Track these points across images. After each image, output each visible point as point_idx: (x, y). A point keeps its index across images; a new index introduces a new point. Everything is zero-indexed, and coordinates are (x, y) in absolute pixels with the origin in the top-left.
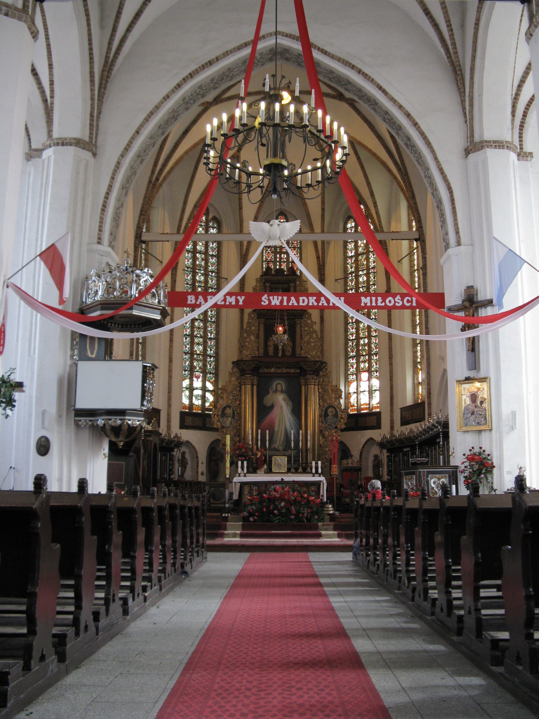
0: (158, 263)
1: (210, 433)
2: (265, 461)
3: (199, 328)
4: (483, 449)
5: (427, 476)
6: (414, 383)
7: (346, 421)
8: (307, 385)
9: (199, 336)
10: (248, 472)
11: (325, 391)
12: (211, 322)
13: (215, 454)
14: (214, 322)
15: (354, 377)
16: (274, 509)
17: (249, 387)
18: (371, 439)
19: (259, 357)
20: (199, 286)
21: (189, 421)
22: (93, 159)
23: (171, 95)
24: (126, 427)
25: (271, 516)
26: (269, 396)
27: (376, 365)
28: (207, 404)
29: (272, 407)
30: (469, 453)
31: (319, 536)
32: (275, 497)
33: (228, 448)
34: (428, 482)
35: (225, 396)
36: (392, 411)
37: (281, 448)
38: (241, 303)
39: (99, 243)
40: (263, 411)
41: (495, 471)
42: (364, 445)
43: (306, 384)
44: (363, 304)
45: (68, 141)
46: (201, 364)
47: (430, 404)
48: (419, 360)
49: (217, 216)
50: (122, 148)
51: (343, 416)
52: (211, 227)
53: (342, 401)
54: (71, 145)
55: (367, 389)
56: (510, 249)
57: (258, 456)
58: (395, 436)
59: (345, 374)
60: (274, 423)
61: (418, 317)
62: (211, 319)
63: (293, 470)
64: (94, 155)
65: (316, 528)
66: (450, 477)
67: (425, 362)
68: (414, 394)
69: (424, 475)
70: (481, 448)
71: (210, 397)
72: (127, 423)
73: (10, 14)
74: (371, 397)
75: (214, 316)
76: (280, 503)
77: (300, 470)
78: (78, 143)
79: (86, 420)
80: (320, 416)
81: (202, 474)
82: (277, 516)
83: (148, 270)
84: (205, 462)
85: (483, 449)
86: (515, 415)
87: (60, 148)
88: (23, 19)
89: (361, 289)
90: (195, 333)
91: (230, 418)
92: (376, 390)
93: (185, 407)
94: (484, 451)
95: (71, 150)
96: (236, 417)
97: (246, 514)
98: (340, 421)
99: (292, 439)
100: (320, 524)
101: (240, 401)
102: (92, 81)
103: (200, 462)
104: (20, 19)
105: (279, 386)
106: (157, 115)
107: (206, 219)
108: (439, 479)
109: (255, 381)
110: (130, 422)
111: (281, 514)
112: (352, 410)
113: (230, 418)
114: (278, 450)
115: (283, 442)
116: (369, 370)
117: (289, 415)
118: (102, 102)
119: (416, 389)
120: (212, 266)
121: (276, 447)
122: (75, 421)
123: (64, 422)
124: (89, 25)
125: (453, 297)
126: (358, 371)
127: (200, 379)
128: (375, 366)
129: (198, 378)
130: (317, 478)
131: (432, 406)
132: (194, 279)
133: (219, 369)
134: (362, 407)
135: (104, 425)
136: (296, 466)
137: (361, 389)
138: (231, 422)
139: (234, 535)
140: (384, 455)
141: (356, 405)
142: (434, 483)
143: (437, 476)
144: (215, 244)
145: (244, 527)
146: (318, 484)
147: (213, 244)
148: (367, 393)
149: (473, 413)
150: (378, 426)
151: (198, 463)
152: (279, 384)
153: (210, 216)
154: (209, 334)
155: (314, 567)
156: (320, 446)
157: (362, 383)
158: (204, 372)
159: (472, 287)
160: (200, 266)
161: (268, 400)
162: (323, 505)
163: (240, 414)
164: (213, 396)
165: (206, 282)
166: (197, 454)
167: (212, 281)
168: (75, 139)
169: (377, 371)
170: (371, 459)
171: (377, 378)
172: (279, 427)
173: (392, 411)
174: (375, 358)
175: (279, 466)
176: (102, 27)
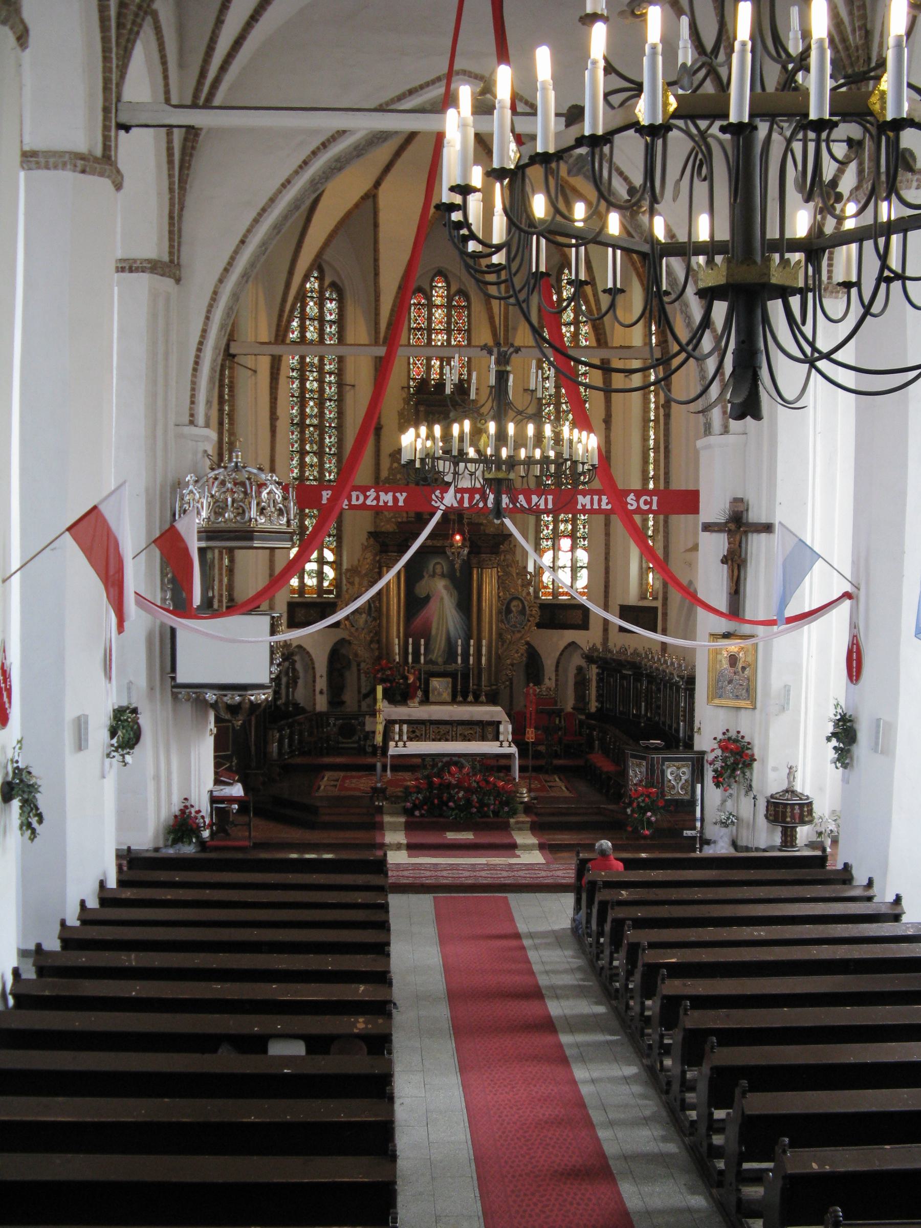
0: (250, 372)
3: (312, 466)
4: (742, 734)
5: (663, 764)
6: (641, 568)
7: (537, 620)
8: (482, 569)
9: (311, 478)
10: (410, 739)
11: (508, 574)
12: (330, 454)
14: (334, 454)
15: (550, 543)
16: (449, 800)
19: (408, 522)
20: (311, 399)
21: (300, 614)
22: (176, 287)
23: (294, 178)
24: (247, 706)
25: (445, 808)
26: (424, 582)
27: (584, 528)
28: (326, 584)
29: (428, 598)
30: (720, 737)
32: (450, 783)
34: (663, 772)
35: (357, 580)
37: (440, 660)
38: (401, 503)
39: (192, 423)
41: (755, 765)
42: (563, 651)
44: (579, 507)
45: (138, 264)
46: (308, 385)
47: (665, 615)
48: (650, 533)
49: (338, 281)
50: (220, 269)
51: (534, 612)
52: (328, 299)
54: (143, 272)
55: (569, 564)
56: (800, 540)
57: (410, 681)
58: (610, 651)
59: (536, 539)
60: (431, 623)
61: (651, 467)
62: (330, 449)
64: (178, 281)
66: (693, 765)
67: (660, 537)
68: (641, 584)
69: (658, 763)
70: (738, 732)
72: (249, 700)
73: (88, 169)
74: (574, 577)
75: (333, 446)
76: (458, 793)
77: (470, 698)
78: (153, 267)
79: (188, 693)
80: (499, 612)
81: (321, 692)
82: (453, 809)
83: (272, 477)
84: (325, 674)
85: (742, 734)
86: (789, 691)
87: (126, 275)
88: (107, 174)
89: (564, 406)
90: (307, 474)
91: (364, 616)
92: (582, 567)
94: (743, 737)
95: (145, 277)
98: (529, 621)
99: (459, 651)
100: (512, 821)
102: (170, 162)
104: (101, 175)
105: (438, 567)
106: (272, 212)
107: (321, 286)
108: (678, 768)
110: (252, 698)
111: (458, 807)
112: (544, 594)
113: (364, 616)
115: (444, 651)
116: (573, 536)
117: (454, 611)
118: (185, 190)
119: (645, 576)
120: (330, 364)
121: (434, 658)
122: (173, 693)
123: (158, 703)
124: (166, 78)
125: (713, 507)
126: (556, 536)
128: (582, 530)
130: (506, 750)
131: (668, 617)
132: (302, 387)
133: (343, 529)
134: (561, 590)
135: (216, 701)
137: (560, 563)
138: (366, 621)
141: (551, 587)
142: (671, 774)
143: (676, 764)
144: (334, 327)
146: (509, 756)
147: (331, 327)
148: (568, 570)
149: (730, 682)
151: (314, 677)
152: (438, 563)
153: (327, 283)
154: (327, 475)
155: (532, 955)
157: (561, 554)
159: (741, 500)
160: (312, 365)
161: (421, 589)
164: (334, 569)
165: (321, 390)
166: (313, 663)
167: (330, 388)
168: (149, 261)
169: (584, 539)
170: (572, 672)
171: (585, 549)
172: (438, 629)
174: (583, 517)
176: (182, 66)
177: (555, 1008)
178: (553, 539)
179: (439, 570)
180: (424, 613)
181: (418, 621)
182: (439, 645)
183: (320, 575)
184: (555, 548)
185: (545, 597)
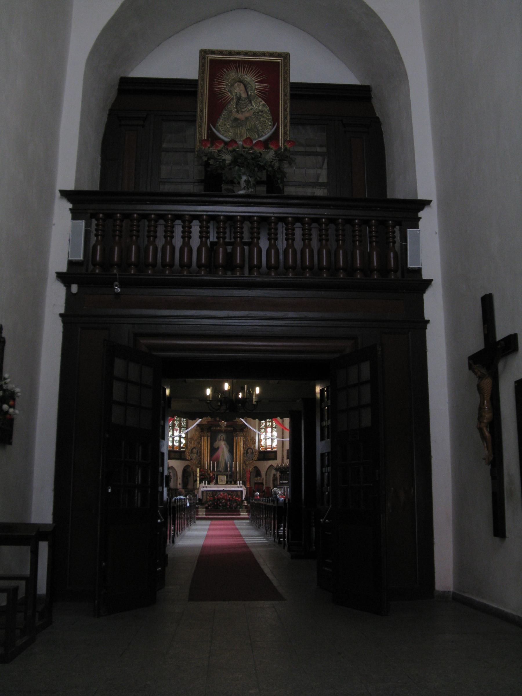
1: (184, 461)
2: (214, 478)
11: (246, 440)
13: (186, 472)
15: (264, 430)
17: (206, 438)
18: (272, 465)
21: (172, 455)
26: (217, 442)
28: (182, 445)
29: (218, 448)
31: (240, 515)
33: (198, 475)
35: (193, 442)
36: (283, 451)
37: (223, 471)
40: (213, 450)
43: (237, 437)
46: (178, 423)
53: (257, 445)
63: (229, 483)
65: (239, 511)
71: (183, 441)
77: (233, 482)
80: (244, 453)
81: (180, 484)
93: (170, 447)
96: (199, 454)
97: (207, 505)
101: (201, 445)
103: (178, 478)
105: (222, 437)
109: (209, 434)
111: (223, 506)
114: (221, 472)
116: (272, 427)
126: (266, 427)
127: (178, 431)
129: (177, 430)
136: (230, 480)
139: (203, 515)
140: (278, 474)
145: (206, 511)
146: (242, 491)
148: (270, 439)
150: (275, 458)
151: (177, 478)
156: (244, 469)
158: (180, 426)
161: (216, 445)
162: (242, 501)
163: (201, 453)
170: (272, 476)
173: (283, 451)
175: (222, 481)
177: (242, 533)
178: (265, 429)
179: (222, 438)
180: (217, 454)
181: (215, 456)
182: (222, 465)
183: (180, 442)
184: (266, 432)
185: (262, 450)
